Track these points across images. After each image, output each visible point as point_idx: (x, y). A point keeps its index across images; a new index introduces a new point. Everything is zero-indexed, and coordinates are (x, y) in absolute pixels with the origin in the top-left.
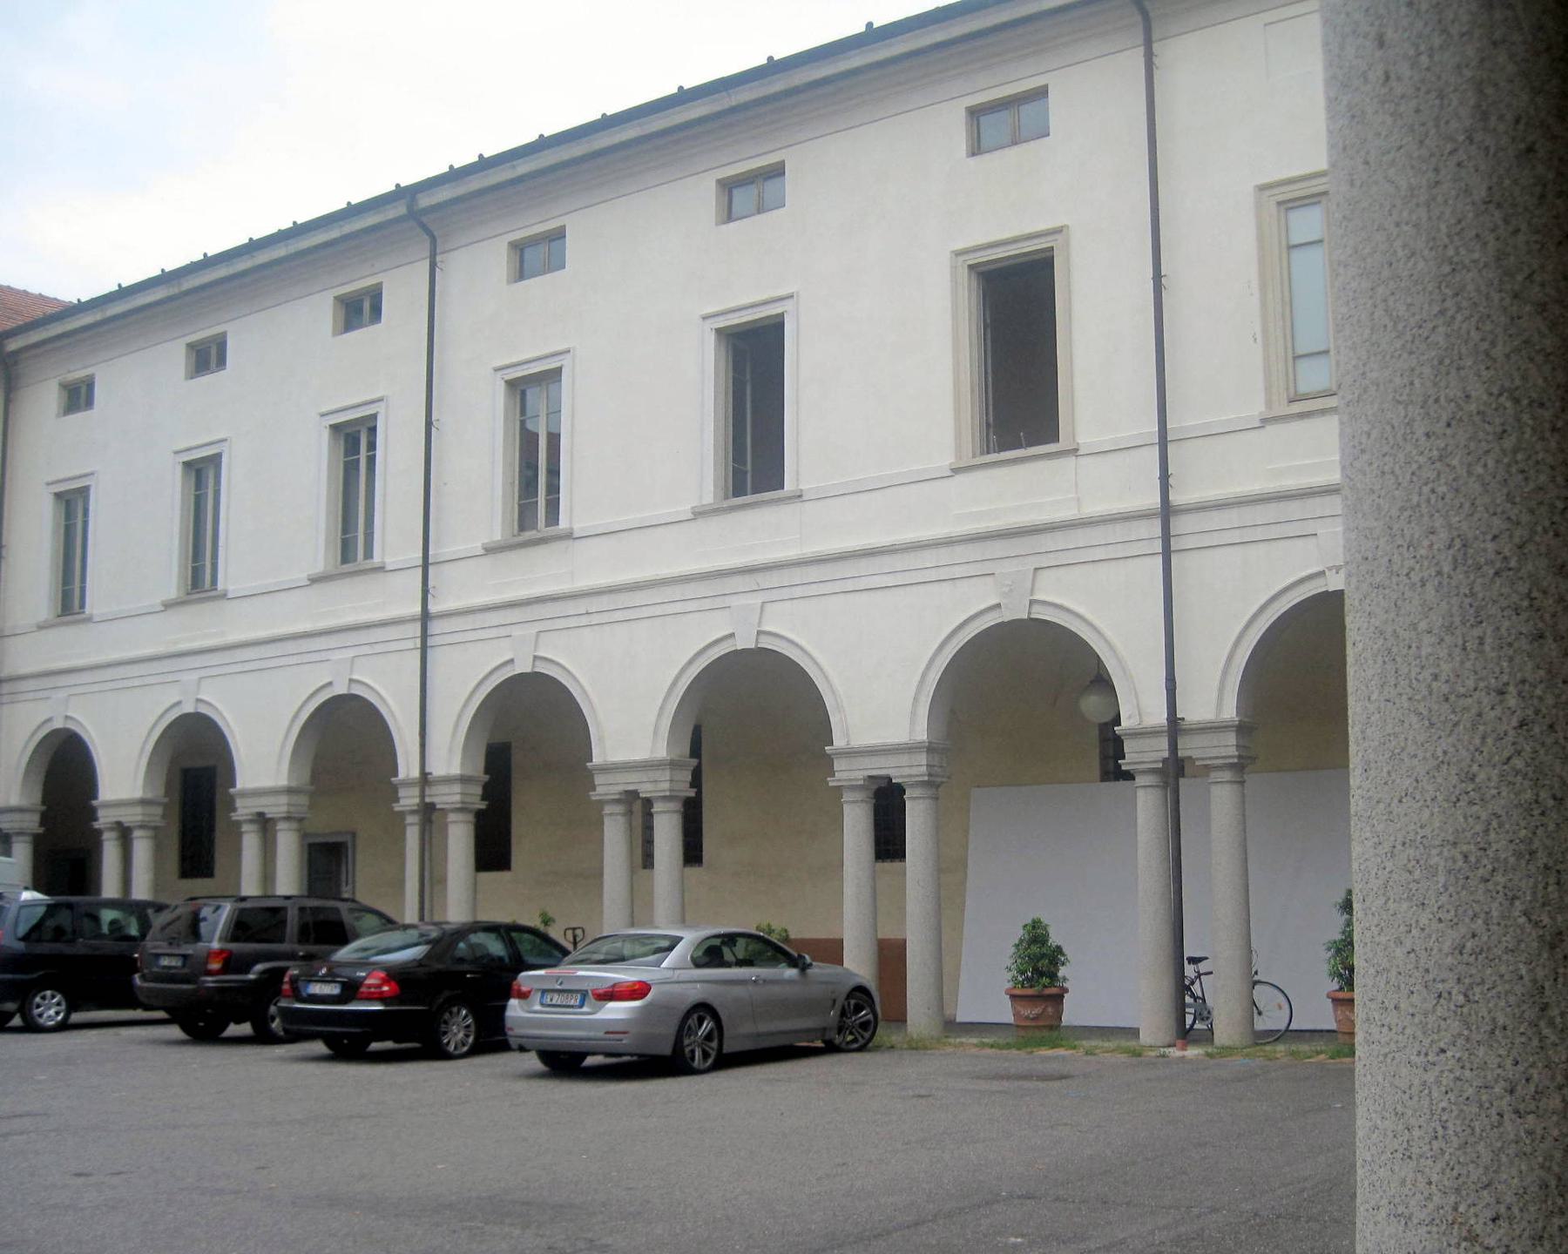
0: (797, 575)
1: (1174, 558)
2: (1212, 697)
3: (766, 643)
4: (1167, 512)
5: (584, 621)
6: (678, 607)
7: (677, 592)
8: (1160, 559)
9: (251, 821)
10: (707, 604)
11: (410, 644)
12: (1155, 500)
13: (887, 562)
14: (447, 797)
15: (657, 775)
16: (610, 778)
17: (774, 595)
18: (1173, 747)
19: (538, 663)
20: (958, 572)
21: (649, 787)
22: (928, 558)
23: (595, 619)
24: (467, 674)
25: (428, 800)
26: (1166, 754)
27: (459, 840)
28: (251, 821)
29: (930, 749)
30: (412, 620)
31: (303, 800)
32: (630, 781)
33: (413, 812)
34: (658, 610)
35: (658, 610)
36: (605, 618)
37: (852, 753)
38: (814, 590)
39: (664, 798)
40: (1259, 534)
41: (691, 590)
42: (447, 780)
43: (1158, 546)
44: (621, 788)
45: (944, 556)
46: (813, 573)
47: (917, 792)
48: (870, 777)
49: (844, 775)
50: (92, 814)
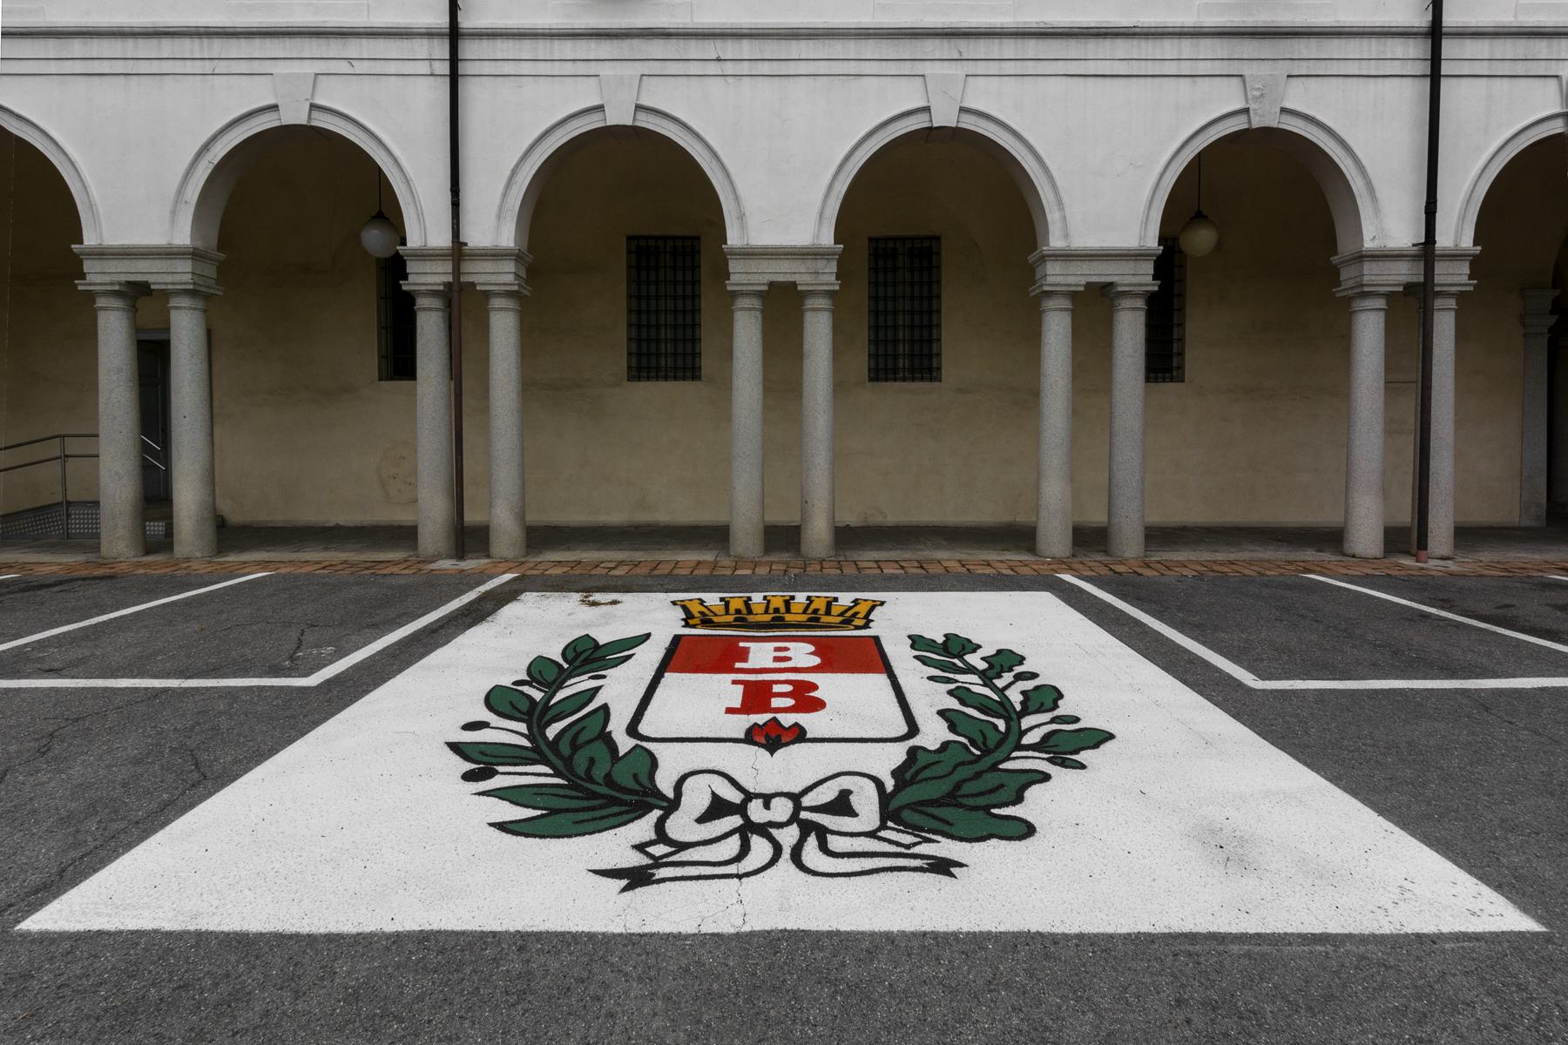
0: (1009, 48)
1: (1445, 85)
2: (494, 223)
3: (969, 123)
4: (454, 34)
5: (713, 68)
6: (852, 68)
7: (851, 48)
8: (447, 80)
9: (116, 294)
10: (893, 68)
11: (1410, 69)
12: (443, 21)
13: (1121, 48)
14: (482, 275)
15: (820, 264)
16: (753, 265)
17: (981, 68)
18: (457, 272)
19: (315, 114)
20: (1203, 68)
21: (807, 279)
22: (1168, 48)
23: (729, 68)
24: (521, 118)
25: (464, 279)
26: (450, 279)
27: (1130, 330)
28: (116, 294)
29: (517, 257)
30: (429, 34)
31: (210, 271)
32: (783, 271)
33: (434, 294)
34: (822, 68)
35: (822, 68)
36: (745, 68)
37: (102, 253)
38: (1030, 67)
39: (186, 292)
40: (1506, 69)
41: (870, 48)
42: (495, 255)
43: (444, 68)
44: (767, 278)
45: (1187, 47)
46: (1032, 48)
47: (184, 302)
48: (128, 283)
49: (743, 279)
50: (74, 267)
